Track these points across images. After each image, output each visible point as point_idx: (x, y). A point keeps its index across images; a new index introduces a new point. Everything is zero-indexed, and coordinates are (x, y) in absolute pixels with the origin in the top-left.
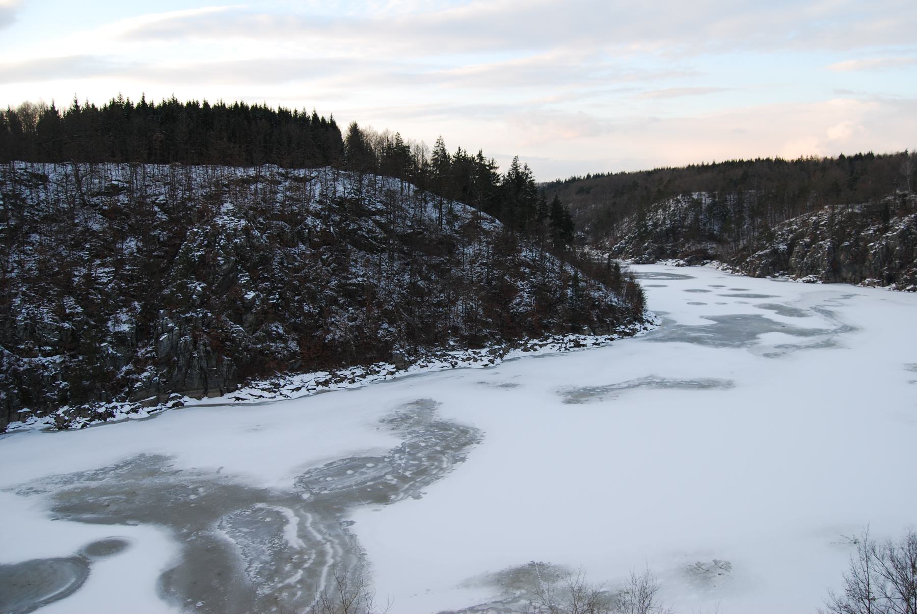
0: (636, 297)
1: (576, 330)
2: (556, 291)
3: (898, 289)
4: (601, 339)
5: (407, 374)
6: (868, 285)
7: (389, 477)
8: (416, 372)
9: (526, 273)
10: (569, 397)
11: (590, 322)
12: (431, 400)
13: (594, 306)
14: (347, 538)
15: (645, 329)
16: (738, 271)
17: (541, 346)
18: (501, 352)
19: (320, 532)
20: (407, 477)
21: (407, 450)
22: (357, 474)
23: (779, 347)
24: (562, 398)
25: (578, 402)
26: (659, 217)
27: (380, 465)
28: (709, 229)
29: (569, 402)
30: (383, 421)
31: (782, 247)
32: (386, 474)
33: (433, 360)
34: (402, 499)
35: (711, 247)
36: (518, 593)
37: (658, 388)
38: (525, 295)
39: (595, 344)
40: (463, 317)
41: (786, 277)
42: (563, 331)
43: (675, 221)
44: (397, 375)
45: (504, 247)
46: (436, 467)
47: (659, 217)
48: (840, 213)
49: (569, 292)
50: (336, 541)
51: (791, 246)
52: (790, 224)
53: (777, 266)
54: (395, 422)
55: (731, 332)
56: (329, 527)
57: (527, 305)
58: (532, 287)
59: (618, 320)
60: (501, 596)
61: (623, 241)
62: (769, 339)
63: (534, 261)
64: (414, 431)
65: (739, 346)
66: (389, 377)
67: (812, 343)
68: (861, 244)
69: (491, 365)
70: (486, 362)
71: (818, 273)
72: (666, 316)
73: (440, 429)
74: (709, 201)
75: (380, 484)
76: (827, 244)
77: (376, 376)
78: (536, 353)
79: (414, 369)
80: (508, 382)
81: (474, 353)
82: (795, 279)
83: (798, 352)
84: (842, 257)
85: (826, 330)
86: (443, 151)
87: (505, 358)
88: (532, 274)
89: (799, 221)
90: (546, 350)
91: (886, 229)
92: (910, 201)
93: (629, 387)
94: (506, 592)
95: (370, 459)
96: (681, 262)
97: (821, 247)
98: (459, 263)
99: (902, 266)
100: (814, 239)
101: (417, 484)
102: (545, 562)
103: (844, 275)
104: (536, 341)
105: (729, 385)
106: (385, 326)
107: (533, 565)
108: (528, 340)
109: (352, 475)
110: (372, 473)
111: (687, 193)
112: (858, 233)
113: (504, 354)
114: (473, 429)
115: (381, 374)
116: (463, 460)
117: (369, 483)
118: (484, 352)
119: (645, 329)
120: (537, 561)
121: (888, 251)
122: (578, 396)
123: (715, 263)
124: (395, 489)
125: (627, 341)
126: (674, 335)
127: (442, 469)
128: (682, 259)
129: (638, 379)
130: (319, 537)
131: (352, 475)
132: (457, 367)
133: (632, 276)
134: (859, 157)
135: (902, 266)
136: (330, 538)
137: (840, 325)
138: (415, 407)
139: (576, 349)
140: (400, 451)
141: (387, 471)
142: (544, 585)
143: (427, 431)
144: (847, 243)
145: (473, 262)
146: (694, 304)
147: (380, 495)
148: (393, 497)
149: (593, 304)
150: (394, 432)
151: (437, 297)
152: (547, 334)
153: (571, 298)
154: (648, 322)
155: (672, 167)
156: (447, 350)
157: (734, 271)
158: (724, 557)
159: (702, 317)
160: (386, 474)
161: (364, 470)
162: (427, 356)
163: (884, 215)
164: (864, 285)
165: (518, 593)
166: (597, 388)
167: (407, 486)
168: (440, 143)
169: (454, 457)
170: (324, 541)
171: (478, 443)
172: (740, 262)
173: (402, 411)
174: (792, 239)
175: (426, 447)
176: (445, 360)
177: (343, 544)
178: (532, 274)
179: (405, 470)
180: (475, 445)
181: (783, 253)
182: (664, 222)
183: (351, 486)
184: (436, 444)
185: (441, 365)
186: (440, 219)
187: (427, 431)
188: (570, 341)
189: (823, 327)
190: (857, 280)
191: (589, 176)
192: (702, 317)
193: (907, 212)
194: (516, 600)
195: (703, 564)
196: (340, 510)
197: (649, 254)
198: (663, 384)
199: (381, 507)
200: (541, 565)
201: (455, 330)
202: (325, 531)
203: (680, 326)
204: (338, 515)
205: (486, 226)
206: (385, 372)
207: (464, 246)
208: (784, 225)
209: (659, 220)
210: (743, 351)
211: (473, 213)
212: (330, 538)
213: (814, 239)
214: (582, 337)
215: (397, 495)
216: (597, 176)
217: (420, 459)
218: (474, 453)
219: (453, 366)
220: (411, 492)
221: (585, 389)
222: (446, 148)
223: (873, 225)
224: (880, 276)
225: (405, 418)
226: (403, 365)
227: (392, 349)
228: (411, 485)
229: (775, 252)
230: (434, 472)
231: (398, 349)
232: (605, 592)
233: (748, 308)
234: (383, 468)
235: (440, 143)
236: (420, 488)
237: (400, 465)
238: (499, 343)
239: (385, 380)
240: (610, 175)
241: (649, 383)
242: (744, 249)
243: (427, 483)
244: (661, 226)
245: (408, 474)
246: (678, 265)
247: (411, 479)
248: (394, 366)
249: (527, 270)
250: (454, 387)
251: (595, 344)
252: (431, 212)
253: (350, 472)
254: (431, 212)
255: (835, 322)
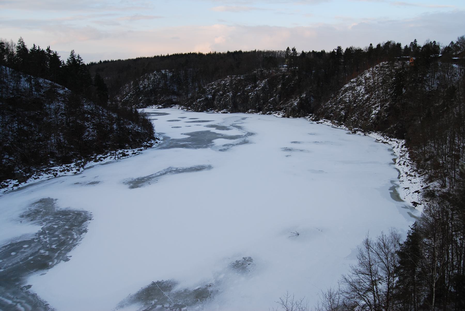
0: (149, 126)
1: (122, 147)
2: (107, 126)
3: (264, 114)
4: (136, 150)
5: (26, 184)
6: (250, 113)
7: (42, 251)
8: (30, 183)
9: (89, 118)
10: (131, 185)
11: (128, 142)
12: (49, 198)
13: (129, 133)
14: (30, 297)
15: (157, 143)
16: (190, 109)
17: (104, 158)
18: (82, 164)
19: (9, 298)
20: (54, 249)
21: (47, 232)
22: (19, 254)
23: (224, 145)
24: (128, 186)
25: (138, 187)
26: (144, 83)
27: (33, 245)
28: (172, 89)
29: (132, 187)
30: (22, 216)
31: (210, 96)
32: (39, 249)
33: (42, 174)
34: (57, 263)
35: (175, 98)
36: (153, 302)
37: (176, 173)
38: (91, 130)
39: (133, 154)
40: (55, 146)
41: (213, 111)
42: (116, 149)
43: (155, 85)
44: (20, 186)
45: (73, 104)
46: (71, 239)
47: (144, 83)
48: (235, 79)
49: (115, 126)
50: (24, 301)
51: (214, 96)
52: (212, 85)
53: (208, 106)
54: (31, 215)
55: (199, 140)
56: (14, 293)
57: (92, 136)
58: (94, 125)
59: (142, 139)
60: (144, 306)
61: (127, 97)
62: (218, 142)
63: (92, 110)
64: (46, 219)
65: (206, 147)
66: (15, 188)
67: (238, 142)
68: (246, 93)
69: (78, 172)
70: (75, 171)
71: (228, 108)
72: (164, 135)
73: (63, 215)
74: (170, 75)
75: (39, 256)
76: (230, 94)
77: (6, 189)
78: (102, 162)
79: (30, 181)
80: (93, 181)
81: (67, 166)
82: (217, 112)
83: (234, 147)
84: (238, 100)
85: (242, 135)
86: (24, 46)
87: (85, 167)
88: (92, 118)
89: (216, 83)
90: (107, 160)
91: (256, 86)
92: (264, 73)
93: (161, 175)
94: (147, 304)
95: (25, 242)
96: (160, 106)
97: (228, 95)
98: (47, 114)
99: (264, 103)
100: (224, 93)
101: (63, 252)
102: (160, 280)
103: (239, 109)
104: (101, 156)
105: (210, 167)
106: (7, 156)
107: (154, 284)
108: (96, 156)
109: (16, 255)
110: (30, 251)
111: (159, 71)
112: (244, 89)
113: (84, 165)
114: (84, 212)
115: (9, 187)
116: (86, 231)
117: (30, 258)
118: (72, 165)
119: (157, 143)
120: (155, 281)
121: (257, 96)
122: (136, 183)
123: (177, 106)
124: (49, 258)
125: (149, 150)
126: (172, 145)
127: (75, 239)
128: (160, 105)
129: (164, 170)
130: (10, 302)
131: (16, 255)
132: (57, 176)
133: (145, 114)
134: (236, 52)
135: (264, 103)
136: (18, 300)
137: (246, 133)
138: (40, 204)
139: (124, 157)
140: (42, 233)
141: (39, 247)
142: (166, 294)
143: (55, 218)
144: (239, 94)
145: (56, 113)
146: (175, 127)
147: (42, 264)
148: (50, 263)
149: (129, 132)
150: (33, 222)
151: (37, 136)
152: (106, 151)
153: (117, 130)
154: (157, 139)
155: (146, 57)
156: (49, 167)
157: (188, 109)
158: (247, 255)
159: (182, 134)
160: (39, 249)
161: (23, 250)
162: (37, 172)
163: (254, 80)
164: (249, 113)
165: (153, 302)
166: (145, 177)
167: (57, 254)
168: (21, 42)
169: (79, 230)
170: (15, 304)
171: (90, 219)
172: (191, 105)
173: (33, 208)
174: (214, 92)
175: (59, 228)
176: (49, 173)
177: (29, 302)
178: (92, 118)
179: (51, 244)
180: (89, 221)
181: (210, 99)
182: (149, 86)
183: (18, 263)
184: (64, 225)
185: (47, 176)
186: (31, 87)
187: (55, 218)
188: (120, 153)
189: (240, 134)
190: (245, 111)
191: (100, 61)
192: (182, 134)
193: (264, 78)
194: (154, 306)
195: (239, 261)
196: (17, 280)
197: (143, 103)
198: (178, 171)
199: (45, 271)
200: (158, 283)
201: (53, 155)
202: (12, 296)
203: (173, 140)
204: (17, 283)
205: (61, 92)
206: (12, 185)
207: (50, 104)
208: (209, 86)
209: (145, 85)
210: (209, 149)
211: (50, 84)
212: (18, 300)
213: (224, 93)
214: (126, 150)
215: (53, 261)
216: (105, 62)
217: (58, 236)
218: (90, 225)
219: (55, 176)
220: (61, 258)
221: (138, 179)
222: (25, 44)
223: (250, 85)
224: (255, 108)
225: (37, 212)
226: (24, 180)
227: (14, 170)
228: (59, 253)
229: (207, 99)
230: (71, 242)
231: (18, 170)
232: (199, 289)
233: (202, 128)
234: (36, 246)
235: (21, 42)
236: (65, 254)
237: (46, 242)
238: (81, 159)
239: (13, 190)
240: (112, 61)
241: (170, 172)
242: (192, 98)
243: (69, 250)
244: (147, 88)
245: (54, 246)
246: (159, 108)
247: (57, 250)
248: (17, 181)
249: (89, 116)
250: (65, 189)
251: (133, 154)
252: (24, 84)
253: (13, 254)
254: (24, 84)
255: (244, 131)
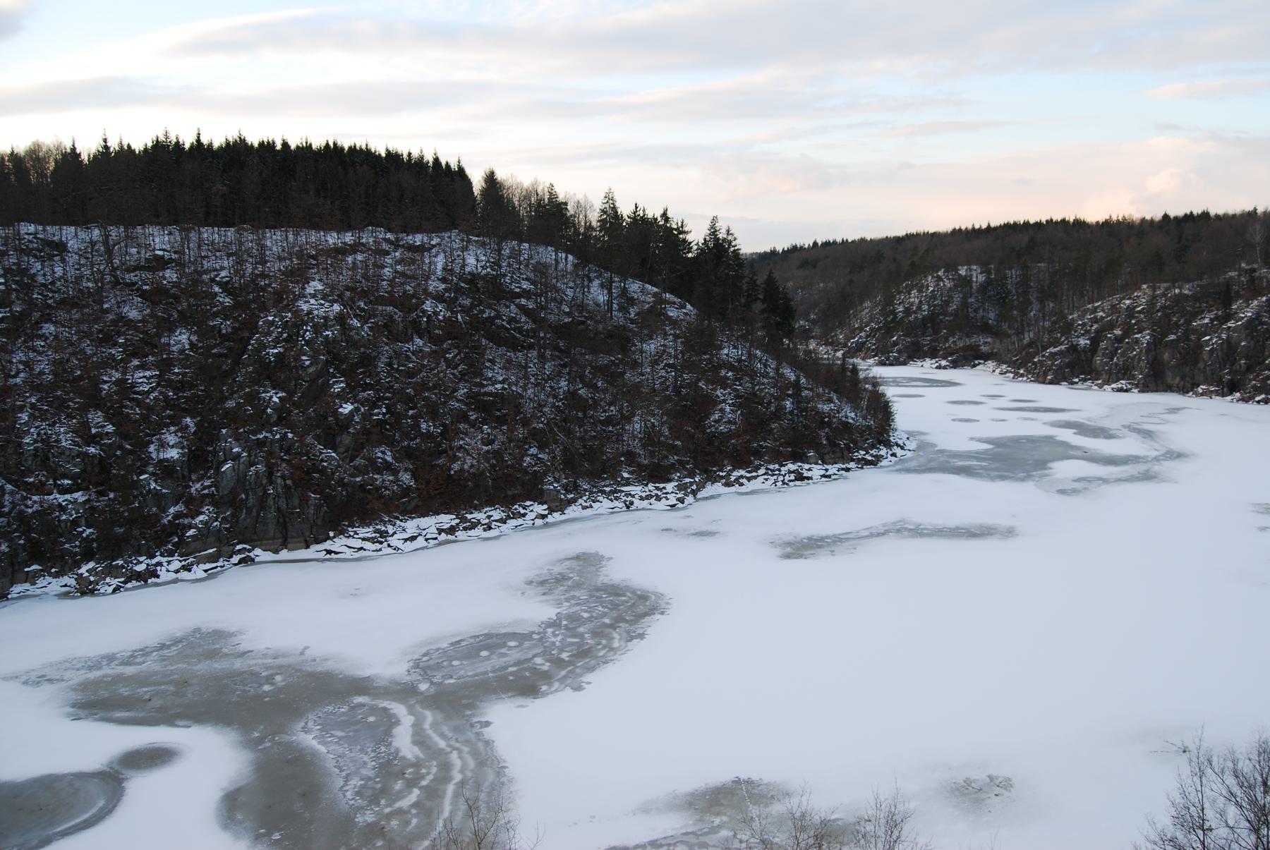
0: (881, 411)
1: (798, 457)
2: (770, 402)
3: (1244, 400)
4: (832, 469)
5: (563, 517)
6: (1202, 394)
7: (538, 660)
8: (576, 515)
9: (728, 378)
10: (789, 550)
11: (817, 446)
12: (596, 554)
13: (822, 424)
14: (480, 745)
15: (894, 455)
16: (1022, 375)
17: (749, 479)
18: (694, 487)
19: (443, 736)
20: (563, 660)
21: (564, 623)
22: (494, 656)
23: (1079, 480)
24: (779, 551)
25: (801, 556)
26: (913, 300)
27: (527, 644)
28: (983, 317)
29: (788, 556)
30: (530, 583)
31: (1083, 342)
32: (535, 656)
33: (600, 498)
34: (556, 691)
35: (985, 342)
36: (717, 821)
37: (912, 536)
38: (728, 409)
39: (823, 476)
40: (641, 439)
41: (1089, 383)
42: (780, 458)
43: (935, 306)
44: (550, 519)
45: (699, 342)
46: (604, 647)
47: (913, 300)
48: (1164, 295)
49: (788, 404)
50: (466, 749)
51: (1095, 341)
52: (1095, 310)
53: (1076, 368)
54: (547, 584)
55: (1012, 460)
56: (456, 730)
57: (729, 422)
58: (737, 397)
59: (855, 443)
60: (694, 825)
61: (863, 334)
62: (1065, 470)
63: (739, 361)
64: (574, 597)
65: (1023, 480)
66: (539, 522)
67: (1125, 475)
68: (1193, 337)
69: (680, 505)
70: (673, 501)
71: (1133, 377)
72: (922, 438)
73: (610, 594)
74: (982, 278)
75: (526, 670)
76: (1145, 338)
77: (520, 521)
78: (743, 489)
79: (573, 511)
80: (704, 529)
81: (657, 488)
82: (1100, 386)
83: (1105, 487)
84: (1166, 356)
85: (1145, 457)
86: (614, 209)
87: (700, 495)
88: (737, 379)
89: (1107, 305)
90: (756, 484)
91: (1228, 317)
92: (1261, 278)
93: (872, 535)
94: (701, 820)
95: (513, 636)
96: (944, 363)
97: (1137, 341)
98: (635, 365)
99: (1249, 369)
100: (1128, 331)
101: (578, 670)
102: (755, 777)
103: (1169, 380)
104: (742, 472)
105: (1009, 533)
106: (533, 451)
107: (738, 782)
108: (732, 471)
109: (488, 658)
110: (515, 655)
111: (951, 267)
112: (1188, 322)
113: (699, 489)
114: (655, 594)
115: (527, 517)
116: (641, 636)
117: (511, 669)
118: (670, 487)
119: (894, 455)
120: (744, 776)
121: (1230, 348)
122: (800, 548)
123: (991, 364)
124: (546, 677)
125: (868, 472)
126: (933, 464)
127: (612, 649)
128: (945, 358)
129: (884, 525)
130: (442, 744)
131: (488, 658)
132: (633, 507)
133: (875, 382)
134: (1189, 218)
135: (1249, 369)
136: (457, 745)
137: (1163, 451)
138: (575, 563)
139: (798, 483)
140: (554, 624)
141: (536, 651)
142: (754, 810)
143: (591, 596)
144: (1173, 337)
145: (655, 363)
146: (960, 420)
147: (527, 685)
148: (544, 688)
149: (822, 421)
150: (545, 598)
151: (605, 411)
152: (757, 462)
153: (791, 413)
154: (898, 445)
155: (931, 231)
156: (619, 484)
157: (1017, 375)
158: (1002, 772)
159: (972, 439)
160: (535, 656)
161: (504, 651)
162: (591, 493)
163: (1224, 298)
164: (1197, 394)
165: (717, 821)
166: (827, 537)
167: (563, 673)
168: (609, 198)
169: (628, 632)
170: (449, 750)
171: (662, 613)
172: (1025, 362)
173: (557, 570)
174: (1097, 331)
175: (590, 619)
176: (617, 499)
177: (475, 754)
178: (737, 379)
179: (561, 650)
180: (657, 616)
181: (1084, 350)
182: (919, 308)
183: (486, 673)
184: (604, 615)
185: (611, 505)
186: (610, 303)
187: (591, 596)
188: (790, 472)
189: (1140, 453)
190: (1186, 387)
191: (815, 243)
192: (972, 439)
193: (1256, 294)
194: (714, 830)
195: (974, 781)
196: (471, 706)
197: (899, 352)
198: (918, 532)
199: (528, 701)
200: (749, 782)
201: (631, 457)
202: (450, 735)
203: (942, 452)
204: (469, 712)
205: (672, 313)
206: (533, 515)
207: (642, 341)
208: (1085, 312)
209: (912, 304)
210: (1029, 486)
211: (655, 295)
212: (457, 745)
213: (1128, 331)
214: (807, 466)
215: (550, 685)
216: (827, 244)
217: (581, 636)
218: (656, 627)
219: (628, 507)
220: (569, 681)
221: (810, 539)
222: (617, 204)
223: (1209, 312)
224: (1219, 382)
225: (561, 579)
226: (559, 505)
227: (542, 483)
228: (569, 672)
229: (1073, 348)
230: (601, 653)
231: (551, 484)
232: (838, 819)
233: (1036, 427)
234: (530, 648)
235: (609, 198)
236: (581, 675)
237: (553, 643)
238: (691, 475)
239: (533, 527)
240: (845, 243)
241: (898, 531)
242: (1030, 344)
243: (591, 669)
244: (915, 312)
245: (565, 656)
246: (939, 367)
247: (569, 663)
248: (545, 506)
249: (730, 374)
250: (628, 536)
251: (823, 476)
252: (597, 294)
253: (484, 653)
254: (597, 294)
255: (1156, 446)
